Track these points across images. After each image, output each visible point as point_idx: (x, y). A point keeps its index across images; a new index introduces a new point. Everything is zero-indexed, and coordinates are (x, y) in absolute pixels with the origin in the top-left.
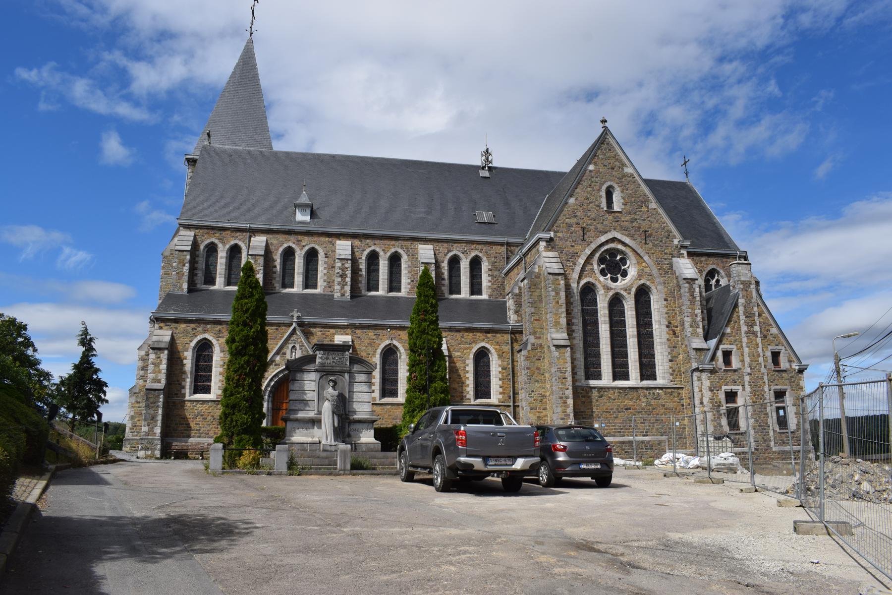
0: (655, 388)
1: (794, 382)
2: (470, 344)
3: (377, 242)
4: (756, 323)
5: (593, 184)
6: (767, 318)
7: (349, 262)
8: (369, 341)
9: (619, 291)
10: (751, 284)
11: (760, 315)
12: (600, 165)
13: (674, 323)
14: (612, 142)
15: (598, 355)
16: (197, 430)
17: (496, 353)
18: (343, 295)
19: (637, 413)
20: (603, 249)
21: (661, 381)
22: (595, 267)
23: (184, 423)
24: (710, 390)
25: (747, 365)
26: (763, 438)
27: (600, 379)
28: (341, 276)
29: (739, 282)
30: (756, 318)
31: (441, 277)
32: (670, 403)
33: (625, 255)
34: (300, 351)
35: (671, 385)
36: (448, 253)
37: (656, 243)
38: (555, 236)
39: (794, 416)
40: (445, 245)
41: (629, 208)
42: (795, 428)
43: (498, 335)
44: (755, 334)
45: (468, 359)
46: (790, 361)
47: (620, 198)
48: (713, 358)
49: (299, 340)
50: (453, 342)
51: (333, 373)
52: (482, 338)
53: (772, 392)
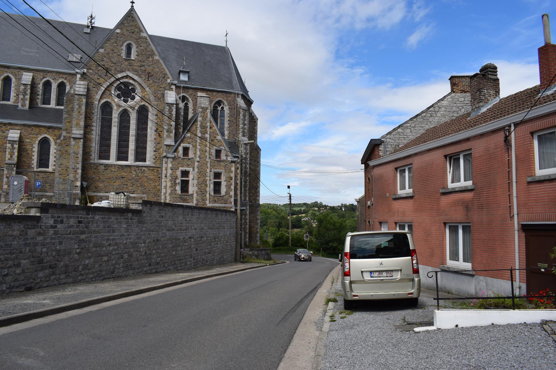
0: (142, 166)
1: (227, 168)
2: (37, 135)
6: (215, 130)
9: (127, 108)
10: (207, 109)
11: (211, 128)
12: (124, 30)
13: (160, 129)
14: (135, 16)
15: (109, 146)
17: (53, 141)
19: (128, 181)
24: (171, 169)
25: (197, 156)
26: (202, 198)
27: (109, 159)
29: (200, 107)
30: (208, 129)
31: (37, 93)
32: (151, 175)
36: (43, 79)
38: (87, 72)
39: (225, 187)
40: (42, 74)
41: (140, 58)
42: (224, 194)
43: (56, 131)
45: (35, 144)
46: (227, 156)
47: (135, 51)
48: (176, 151)
52: (46, 131)
53: (212, 173)
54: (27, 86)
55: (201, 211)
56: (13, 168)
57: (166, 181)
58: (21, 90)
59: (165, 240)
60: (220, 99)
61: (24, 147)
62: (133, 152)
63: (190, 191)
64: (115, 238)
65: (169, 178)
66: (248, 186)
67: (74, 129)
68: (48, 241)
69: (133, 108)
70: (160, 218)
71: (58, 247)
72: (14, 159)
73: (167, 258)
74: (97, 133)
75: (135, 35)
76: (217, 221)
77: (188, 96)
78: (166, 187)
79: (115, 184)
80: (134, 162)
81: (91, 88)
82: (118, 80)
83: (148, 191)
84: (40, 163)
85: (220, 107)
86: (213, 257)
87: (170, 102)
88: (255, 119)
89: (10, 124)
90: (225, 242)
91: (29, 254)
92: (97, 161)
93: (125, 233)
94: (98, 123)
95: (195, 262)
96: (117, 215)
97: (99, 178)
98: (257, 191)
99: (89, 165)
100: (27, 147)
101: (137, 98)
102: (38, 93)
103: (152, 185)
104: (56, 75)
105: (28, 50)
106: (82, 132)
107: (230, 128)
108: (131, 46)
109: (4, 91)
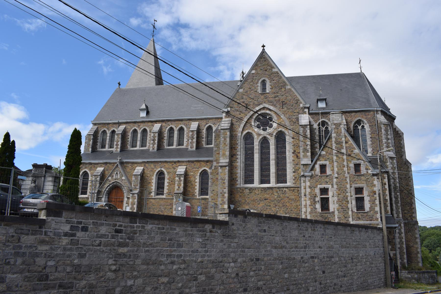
0: (283, 188)
2: (198, 168)
3: (173, 123)
5: (254, 80)
6: (352, 144)
8: (151, 169)
9: (265, 136)
12: (259, 70)
15: (253, 171)
18: (153, 149)
24: (309, 188)
25: (335, 172)
26: (344, 216)
27: (253, 183)
28: (153, 140)
29: (333, 124)
30: (344, 144)
32: (292, 196)
36: (206, 125)
37: (289, 107)
38: (231, 110)
39: (368, 202)
40: (205, 121)
41: (274, 90)
45: (197, 176)
46: (367, 169)
48: (313, 169)
50: (190, 168)
52: (205, 165)
53: (353, 189)
55: (327, 226)
57: (305, 200)
58: (190, 135)
59: (270, 260)
60: (359, 118)
61: (189, 179)
62: (274, 175)
63: (330, 208)
64: (183, 254)
65: (308, 197)
66: (400, 202)
67: (221, 158)
68: (59, 251)
69: (271, 134)
70: (260, 232)
71: (75, 261)
73: (275, 281)
74: (242, 160)
76: (353, 238)
77: (327, 121)
78: (306, 206)
79: (259, 206)
80: (276, 184)
81: (235, 123)
82: (256, 112)
83: (290, 211)
84: (201, 192)
85: (361, 126)
86: (350, 281)
87: (303, 124)
88: (400, 134)
89: (179, 162)
90: (368, 263)
91: (21, 267)
92: (242, 185)
93: (200, 249)
94: (242, 152)
95: (321, 288)
96: (185, 225)
97: (245, 201)
98: (412, 208)
99: (236, 189)
100: (192, 179)
101: (275, 125)
102: (203, 137)
103: (294, 205)
104: (215, 121)
105: (196, 106)
106: (227, 160)
107: (374, 145)
108: (265, 82)
109: (179, 139)
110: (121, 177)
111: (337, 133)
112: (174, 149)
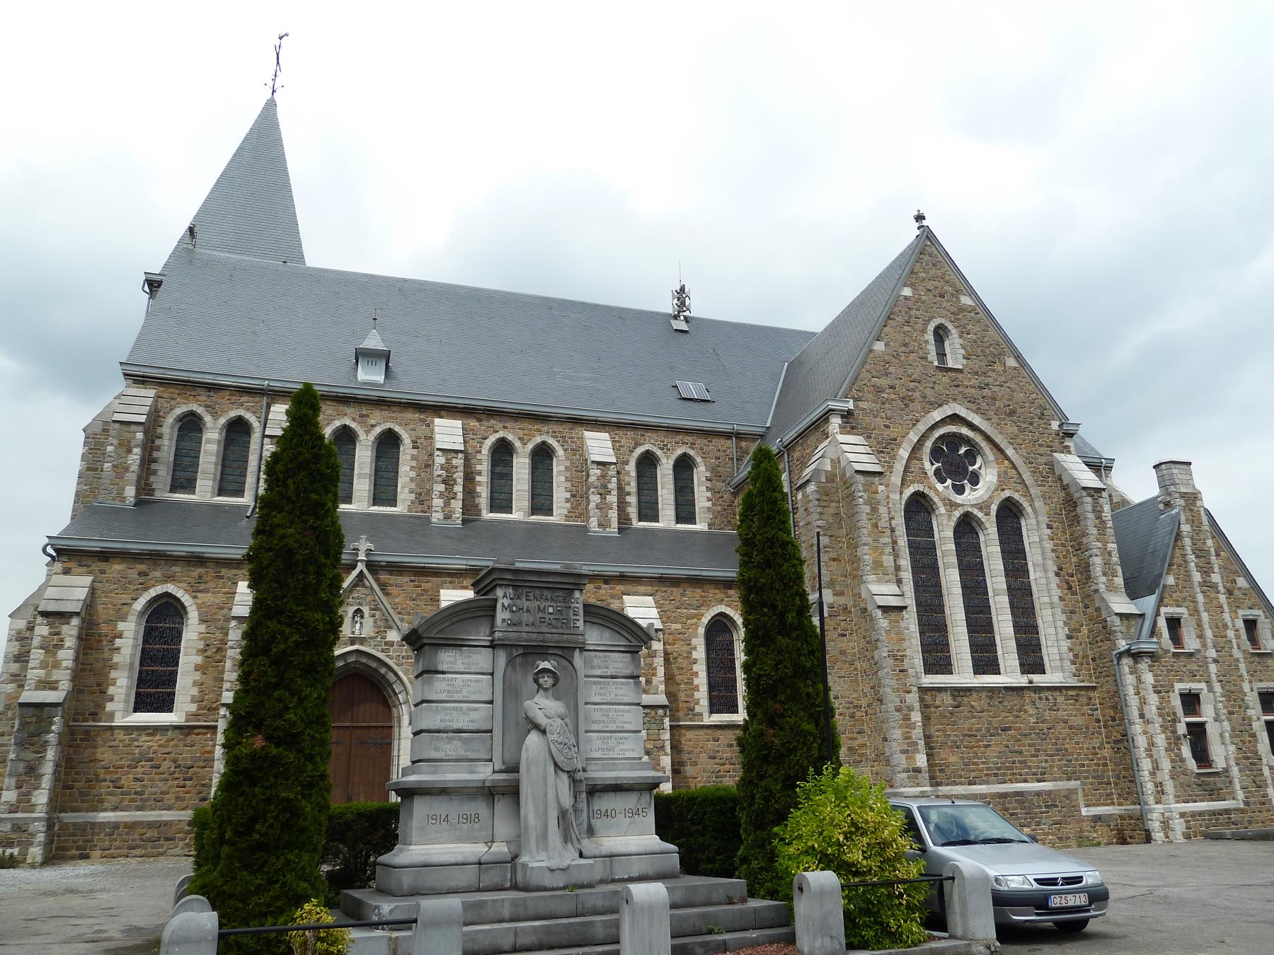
4: (1212, 568)
7: (460, 455)
9: (970, 510)
16: (136, 793)
18: (447, 517)
20: (937, 434)
21: (1051, 678)
22: (927, 465)
23: (108, 777)
25: (1210, 644)
28: (444, 482)
33: (974, 447)
34: (371, 620)
35: (1073, 682)
38: (856, 406)
40: (630, 434)
41: (976, 364)
44: (1213, 587)
45: (696, 636)
49: (369, 598)
51: (540, 651)
54: (609, 469)
56: (662, 720)
72: (657, 687)
75: (948, 301)
79: (989, 752)
110: (381, 633)
111: (1191, 521)
112: (197, 505)
